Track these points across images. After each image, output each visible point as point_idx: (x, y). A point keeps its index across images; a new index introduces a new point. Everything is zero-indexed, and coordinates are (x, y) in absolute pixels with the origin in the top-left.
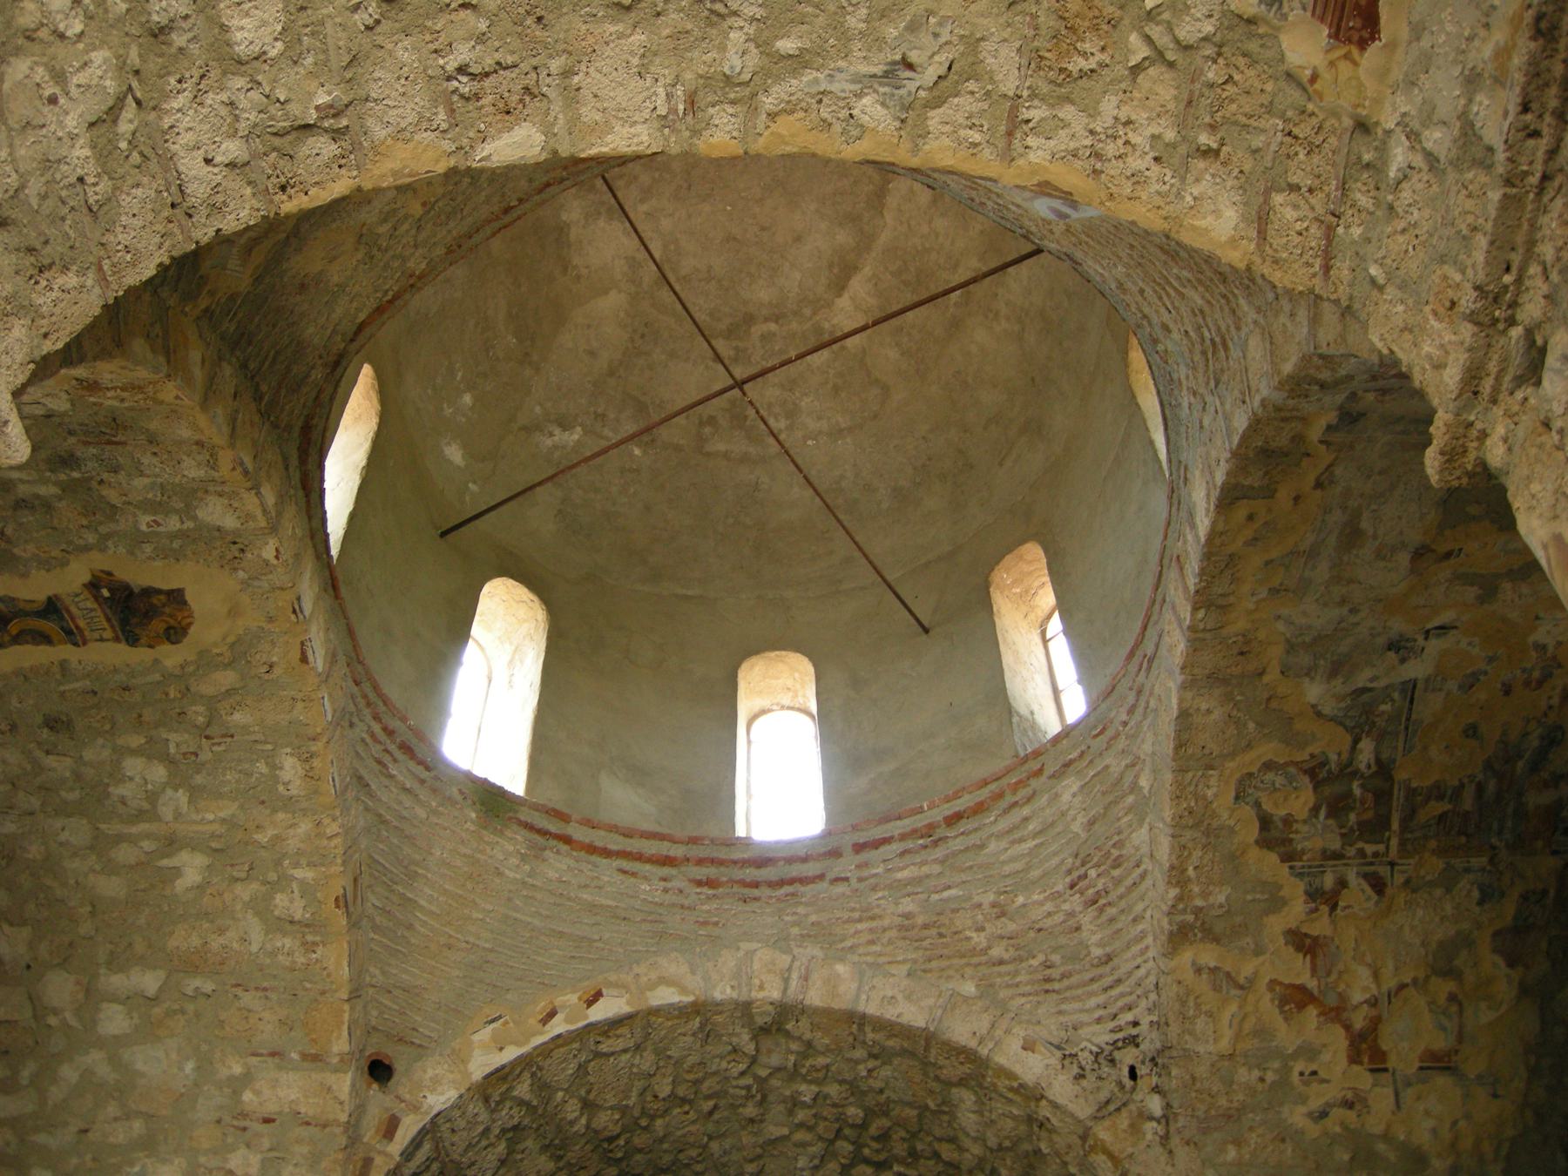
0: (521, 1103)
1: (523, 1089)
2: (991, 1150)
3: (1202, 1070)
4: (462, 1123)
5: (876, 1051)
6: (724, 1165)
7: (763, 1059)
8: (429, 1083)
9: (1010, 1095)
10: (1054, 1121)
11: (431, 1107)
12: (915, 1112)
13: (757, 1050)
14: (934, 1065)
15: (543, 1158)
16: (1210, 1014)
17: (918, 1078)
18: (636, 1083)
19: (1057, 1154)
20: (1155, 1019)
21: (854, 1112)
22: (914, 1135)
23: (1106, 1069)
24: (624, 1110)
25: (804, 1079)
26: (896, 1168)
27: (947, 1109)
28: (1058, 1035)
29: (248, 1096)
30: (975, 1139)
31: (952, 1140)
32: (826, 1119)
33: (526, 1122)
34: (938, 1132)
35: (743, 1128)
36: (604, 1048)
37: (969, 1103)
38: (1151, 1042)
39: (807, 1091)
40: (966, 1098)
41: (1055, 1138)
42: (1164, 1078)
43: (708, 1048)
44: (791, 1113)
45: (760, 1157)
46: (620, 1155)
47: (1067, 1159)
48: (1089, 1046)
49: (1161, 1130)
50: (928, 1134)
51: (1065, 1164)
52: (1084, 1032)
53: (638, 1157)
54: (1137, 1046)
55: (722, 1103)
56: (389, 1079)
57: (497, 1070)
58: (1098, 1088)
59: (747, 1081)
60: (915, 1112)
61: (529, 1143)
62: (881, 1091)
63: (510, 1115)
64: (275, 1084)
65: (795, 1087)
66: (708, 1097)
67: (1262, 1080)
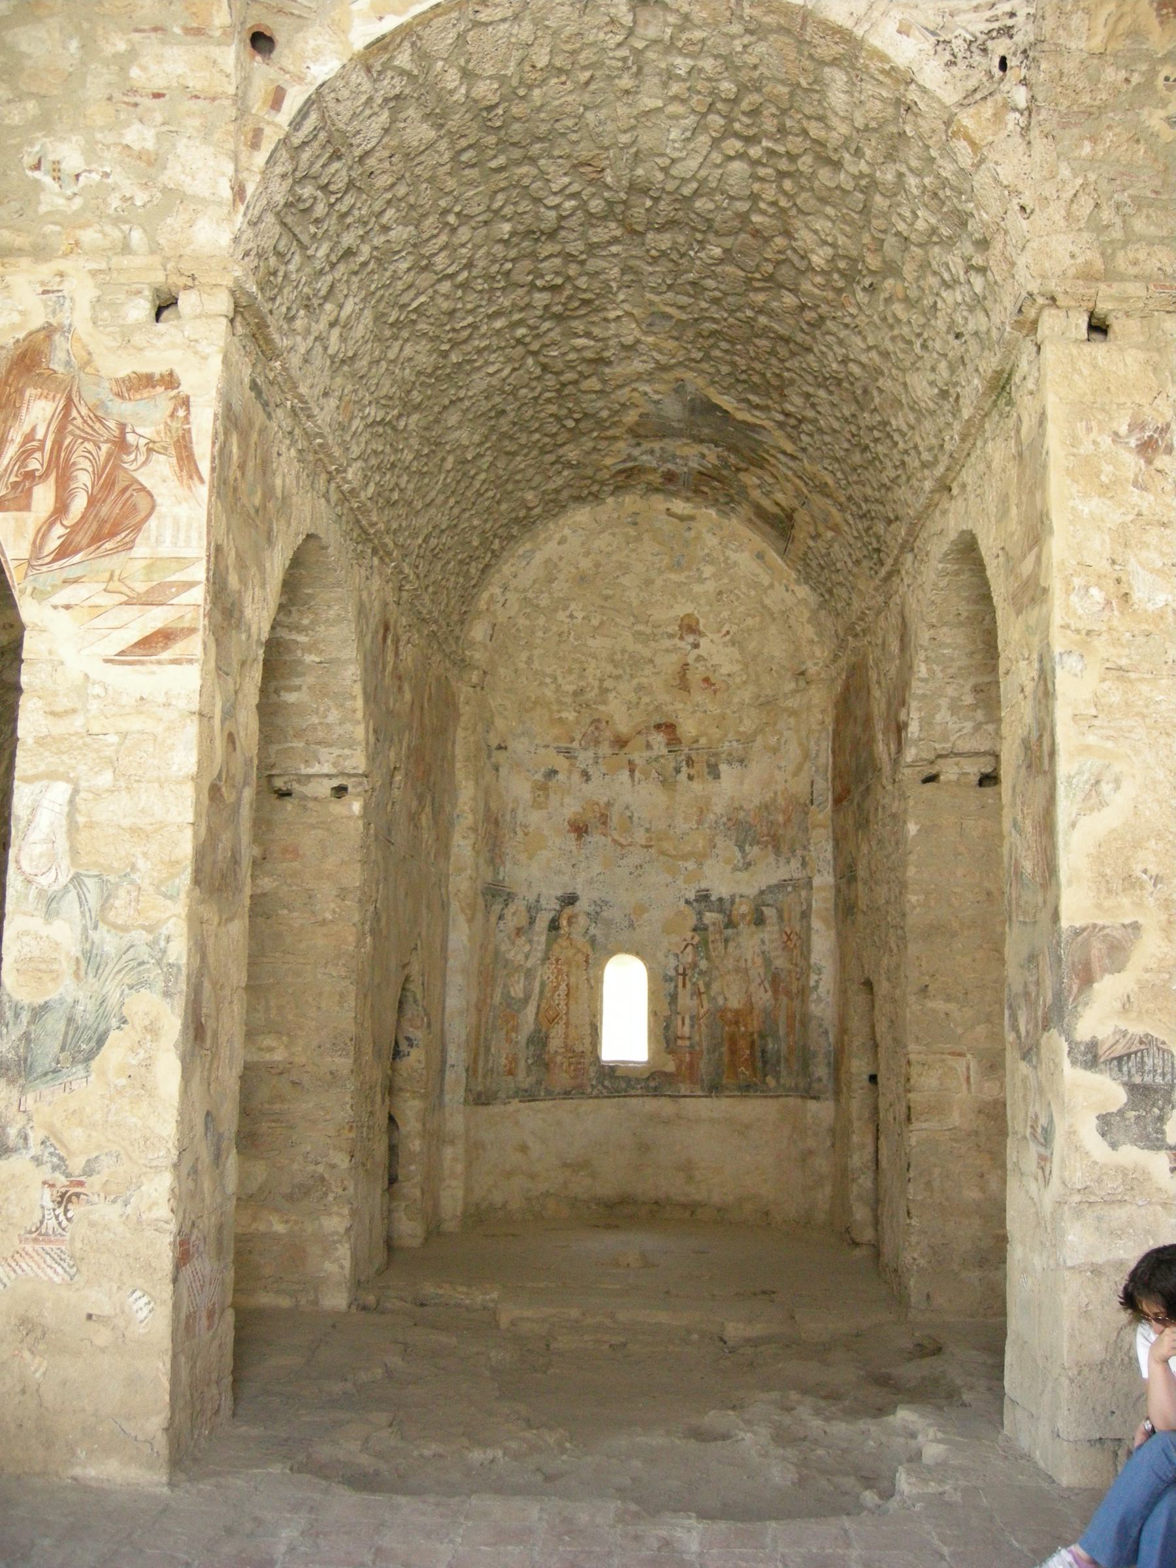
0: (402, 72)
1: (403, 59)
2: (858, 130)
3: (1070, 66)
4: (345, 93)
5: (752, 27)
6: (599, 135)
7: (640, 31)
8: (310, 54)
9: (881, 78)
10: (921, 105)
11: (315, 78)
12: (786, 90)
13: (635, 22)
14: (810, 43)
15: (425, 126)
16: (1087, 11)
17: (793, 55)
18: (514, 53)
19: (921, 137)
20: (1032, 11)
21: (727, 87)
22: (784, 112)
23: (977, 58)
24: (502, 80)
25: (680, 52)
26: (765, 143)
27: (818, 87)
28: (933, 21)
29: (135, 72)
30: (844, 119)
31: (821, 119)
32: (699, 93)
33: (407, 91)
34: (808, 110)
35: (619, 99)
36: (482, 17)
37: (840, 83)
38: (1022, 38)
39: (682, 64)
40: (837, 78)
41: (920, 121)
42: (1033, 71)
43: (586, 19)
44: (665, 85)
45: (633, 128)
46: (498, 124)
47: (930, 142)
48: (964, 34)
49: (1023, 121)
50: (798, 111)
51: (928, 147)
52: (960, 19)
53: (516, 126)
54: (1011, 37)
55: (598, 74)
56: (271, 51)
57: (378, 40)
58: (968, 76)
59: (624, 52)
60: (786, 90)
61: (411, 112)
62: (755, 67)
63: (391, 85)
64: (160, 59)
65: (670, 59)
66: (585, 68)
67: (1127, 80)
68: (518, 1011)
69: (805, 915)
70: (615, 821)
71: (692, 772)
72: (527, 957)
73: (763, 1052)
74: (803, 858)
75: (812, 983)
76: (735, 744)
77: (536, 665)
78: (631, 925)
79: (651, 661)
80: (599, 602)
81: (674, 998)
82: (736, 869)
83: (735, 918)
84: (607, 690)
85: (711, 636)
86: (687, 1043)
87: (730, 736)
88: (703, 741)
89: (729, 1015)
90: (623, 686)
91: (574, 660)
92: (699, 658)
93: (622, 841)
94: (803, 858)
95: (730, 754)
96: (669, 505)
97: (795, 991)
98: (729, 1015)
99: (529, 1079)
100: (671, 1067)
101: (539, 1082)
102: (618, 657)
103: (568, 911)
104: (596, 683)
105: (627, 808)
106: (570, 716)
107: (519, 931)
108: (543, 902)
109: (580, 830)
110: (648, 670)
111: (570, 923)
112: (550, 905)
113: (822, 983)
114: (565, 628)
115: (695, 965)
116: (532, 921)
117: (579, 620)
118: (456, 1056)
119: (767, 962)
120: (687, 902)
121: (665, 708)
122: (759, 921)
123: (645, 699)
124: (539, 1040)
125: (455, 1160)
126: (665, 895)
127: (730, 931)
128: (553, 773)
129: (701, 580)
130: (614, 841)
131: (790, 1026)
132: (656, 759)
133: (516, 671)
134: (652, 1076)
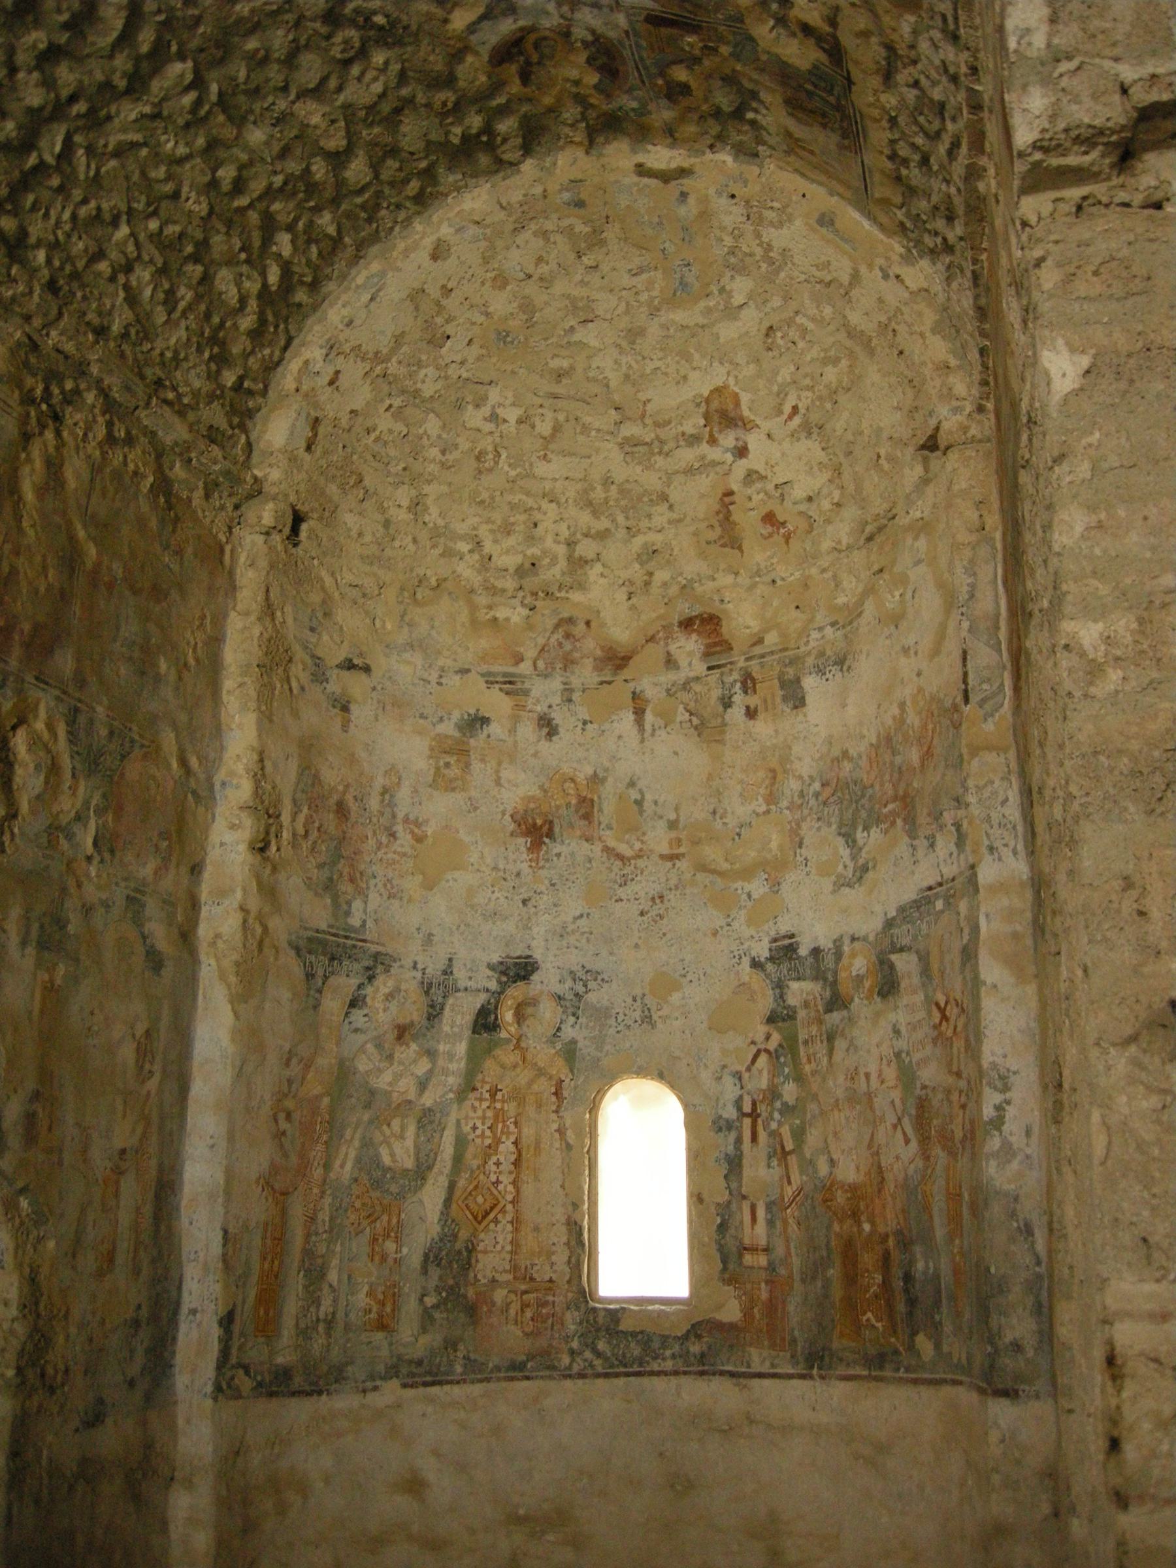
68: (401, 1196)
69: (969, 955)
70: (608, 809)
71: (753, 701)
72: (423, 1086)
73: (908, 1278)
74: (958, 826)
75: (988, 1112)
76: (829, 631)
77: (433, 515)
78: (647, 1019)
79: (664, 497)
80: (546, 386)
81: (734, 1164)
82: (841, 884)
83: (845, 988)
84: (584, 562)
85: (766, 426)
86: (763, 1260)
87: (821, 618)
88: (771, 639)
89: (841, 1198)
90: (613, 551)
91: (513, 507)
92: (751, 477)
93: (623, 849)
94: (958, 826)
95: (822, 654)
96: (640, 158)
97: (959, 1134)
98: (841, 1198)
99: (424, 1340)
100: (731, 1312)
101: (451, 1344)
102: (598, 494)
103: (517, 992)
104: (562, 550)
105: (632, 784)
106: (514, 614)
107: (402, 1032)
108: (460, 975)
109: (537, 831)
110: (661, 515)
111: (520, 1017)
112: (476, 981)
113: (1011, 1112)
114: (487, 444)
115: (773, 1093)
116: (434, 1013)
117: (511, 427)
118: (201, 1291)
119: (907, 1076)
120: (756, 964)
121: (699, 589)
122: (888, 987)
123: (661, 576)
124: (452, 1258)
126: (709, 953)
127: (836, 1017)
128: (477, 722)
129: (732, 312)
130: (607, 850)
131: (954, 1219)
132: (686, 686)
133: (387, 524)
134: (695, 1331)
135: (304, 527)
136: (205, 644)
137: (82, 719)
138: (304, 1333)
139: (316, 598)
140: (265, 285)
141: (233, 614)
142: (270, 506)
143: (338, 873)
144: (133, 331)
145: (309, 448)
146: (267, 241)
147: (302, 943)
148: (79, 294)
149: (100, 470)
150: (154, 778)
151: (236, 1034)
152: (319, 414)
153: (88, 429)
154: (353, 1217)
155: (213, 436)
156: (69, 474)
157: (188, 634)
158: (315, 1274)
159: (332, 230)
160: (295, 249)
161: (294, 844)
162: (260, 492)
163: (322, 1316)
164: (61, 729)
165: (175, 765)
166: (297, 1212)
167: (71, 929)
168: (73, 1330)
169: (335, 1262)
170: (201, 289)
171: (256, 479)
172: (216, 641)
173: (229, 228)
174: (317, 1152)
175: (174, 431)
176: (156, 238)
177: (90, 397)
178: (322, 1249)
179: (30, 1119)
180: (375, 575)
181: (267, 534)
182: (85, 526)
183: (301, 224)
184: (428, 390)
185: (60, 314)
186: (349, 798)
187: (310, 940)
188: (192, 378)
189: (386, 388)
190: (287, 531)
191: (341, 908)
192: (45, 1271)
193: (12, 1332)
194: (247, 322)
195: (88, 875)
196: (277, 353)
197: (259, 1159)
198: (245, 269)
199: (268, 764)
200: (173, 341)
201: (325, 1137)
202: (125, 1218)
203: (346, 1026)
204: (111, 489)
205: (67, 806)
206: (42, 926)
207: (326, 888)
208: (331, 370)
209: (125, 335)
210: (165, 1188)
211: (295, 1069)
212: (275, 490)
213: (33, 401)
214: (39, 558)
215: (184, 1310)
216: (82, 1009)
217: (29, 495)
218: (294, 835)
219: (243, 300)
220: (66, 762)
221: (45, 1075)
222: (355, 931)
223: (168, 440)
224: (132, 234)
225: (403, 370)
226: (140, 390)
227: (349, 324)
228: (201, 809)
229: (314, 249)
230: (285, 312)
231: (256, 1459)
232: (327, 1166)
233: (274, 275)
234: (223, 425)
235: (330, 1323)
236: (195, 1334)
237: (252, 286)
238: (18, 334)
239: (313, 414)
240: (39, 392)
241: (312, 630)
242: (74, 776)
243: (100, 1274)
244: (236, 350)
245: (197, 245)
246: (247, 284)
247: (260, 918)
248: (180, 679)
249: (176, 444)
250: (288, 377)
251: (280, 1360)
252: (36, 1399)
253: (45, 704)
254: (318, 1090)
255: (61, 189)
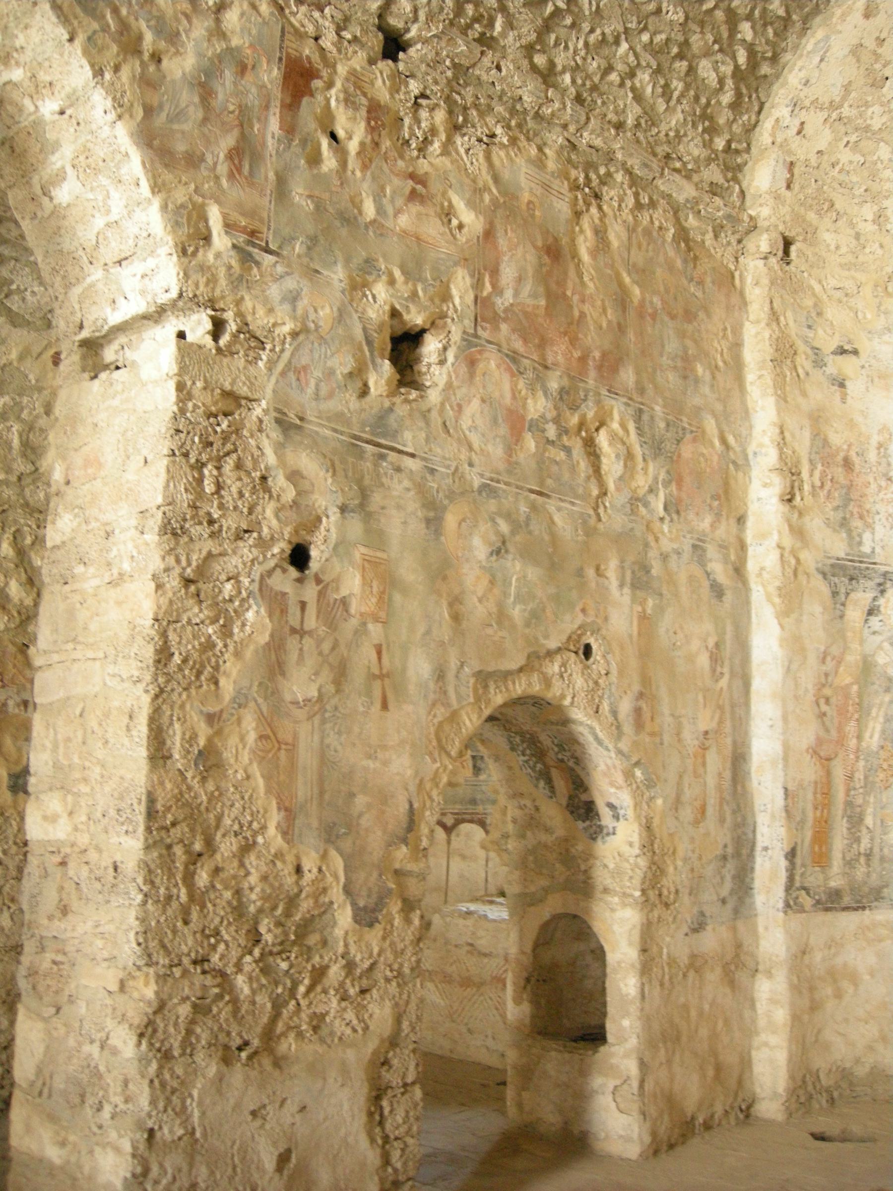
118: (771, 835)
125: (772, 1001)
133: (857, 236)
135: (793, 249)
136: (730, 349)
137: (645, 417)
138: (850, 864)
139: (809, 302)
140: (737, 67)
141: (747, 324)
142: (765, 236)
143: (849, 513)
144: (643, 121)
145: (788, 187)
146: (733, 30)
147: (827, 569)
148: (599, 102)
149: (634, 230)
150: (703, 455)
151: (783, 641)
152: (793, 159)
153: (621, 200)
154: (882, 775)
155: (714, 190)
156: (612, 236)
157: (716, 344)
158: (856, 820)
159: (781, 12)
160: (755, 33)
161: (814, 493)
162: (756, 227)
163: (862, 851)
164: (631, 426)
165: (717, 443)
166: (839, 773)
167: (654, 572)
168: (679, 863)
169: (870, 810)
170: (688, 79)
171: (751, 217)
172: (737, 346)
173: (702, 27)
174: (851, 728)
175: (684, 191)
176: (649, 47)
177: (619, 177)
178: (859, 801)
179: (638, 711)
180: (854, 278)
181: (766, 258)
182: (629, 274)
183: (757, 12)
184: (876, 124)
185: (588, 119)
186: (852, 454)
187: (832, 566)
188: (692, 149)
189: (843, 129)
190: (780, 253)
191: (854, 540)
192: (656, 822)
193: (637, 865)
194: (727, 98)
195: (663, 533)
196: (754, 118)
197: (807, 736)
198: (719, 57)
199: (787, 434)
200: (674, 123)
201: (856, 716)
202: (711, 781)
203: (866, 631)
204: (645, 244)
205: (642, 482)
206: (633, 572)
207: (842, 525)
208: (797, 123)
209: (638, 126)
210: (739, 759)
211: (830, 665)
212: (766, 224)
213: (578, 188)
214: (599, 303)
215: (759, 848)
216: (667, 630)
217: (585, 257)
218: (813, 486)
219: (721, 81)
220: (638, 451)
221: (646, 680)
222: (868, 557)
223: (681, 199)
224: (631, 48)
225: (854, 112)
226: (655, 165)
227: (806, 83)
228: (740, 474)
229: (770, 31)
230: (754, 84)
231: (818, 957)
232: (859, 738)
233: (742, 57)
234: (721, 181)
235: (868, 856)
236: (768, 865)
237: (727, 69)
238: (560, 140)
239: (789, 159)
240: (581, 180)
241: (809, 327)
242: (644, 460)
243: (696, 823)
244: (722, 121)
245: (680, 46)
246: (723, 68)
247: (793, 552)
248: (714, 378)
249: (687, 201)
250: (764, 135)
251: (833, 884)
252: (656, 913)
253: (617, 409)
254: (848, 680)
255: (573, 25)
